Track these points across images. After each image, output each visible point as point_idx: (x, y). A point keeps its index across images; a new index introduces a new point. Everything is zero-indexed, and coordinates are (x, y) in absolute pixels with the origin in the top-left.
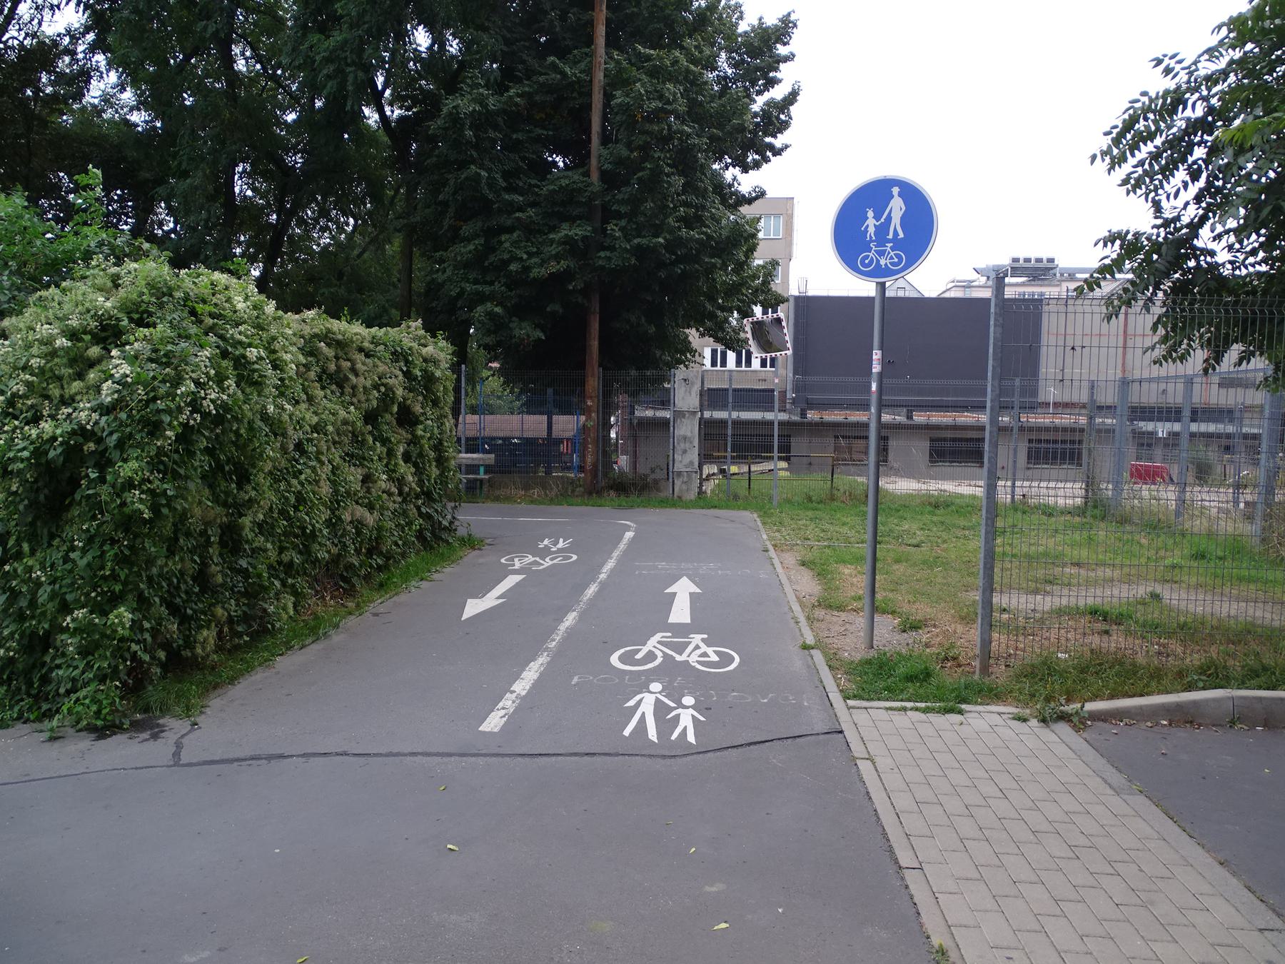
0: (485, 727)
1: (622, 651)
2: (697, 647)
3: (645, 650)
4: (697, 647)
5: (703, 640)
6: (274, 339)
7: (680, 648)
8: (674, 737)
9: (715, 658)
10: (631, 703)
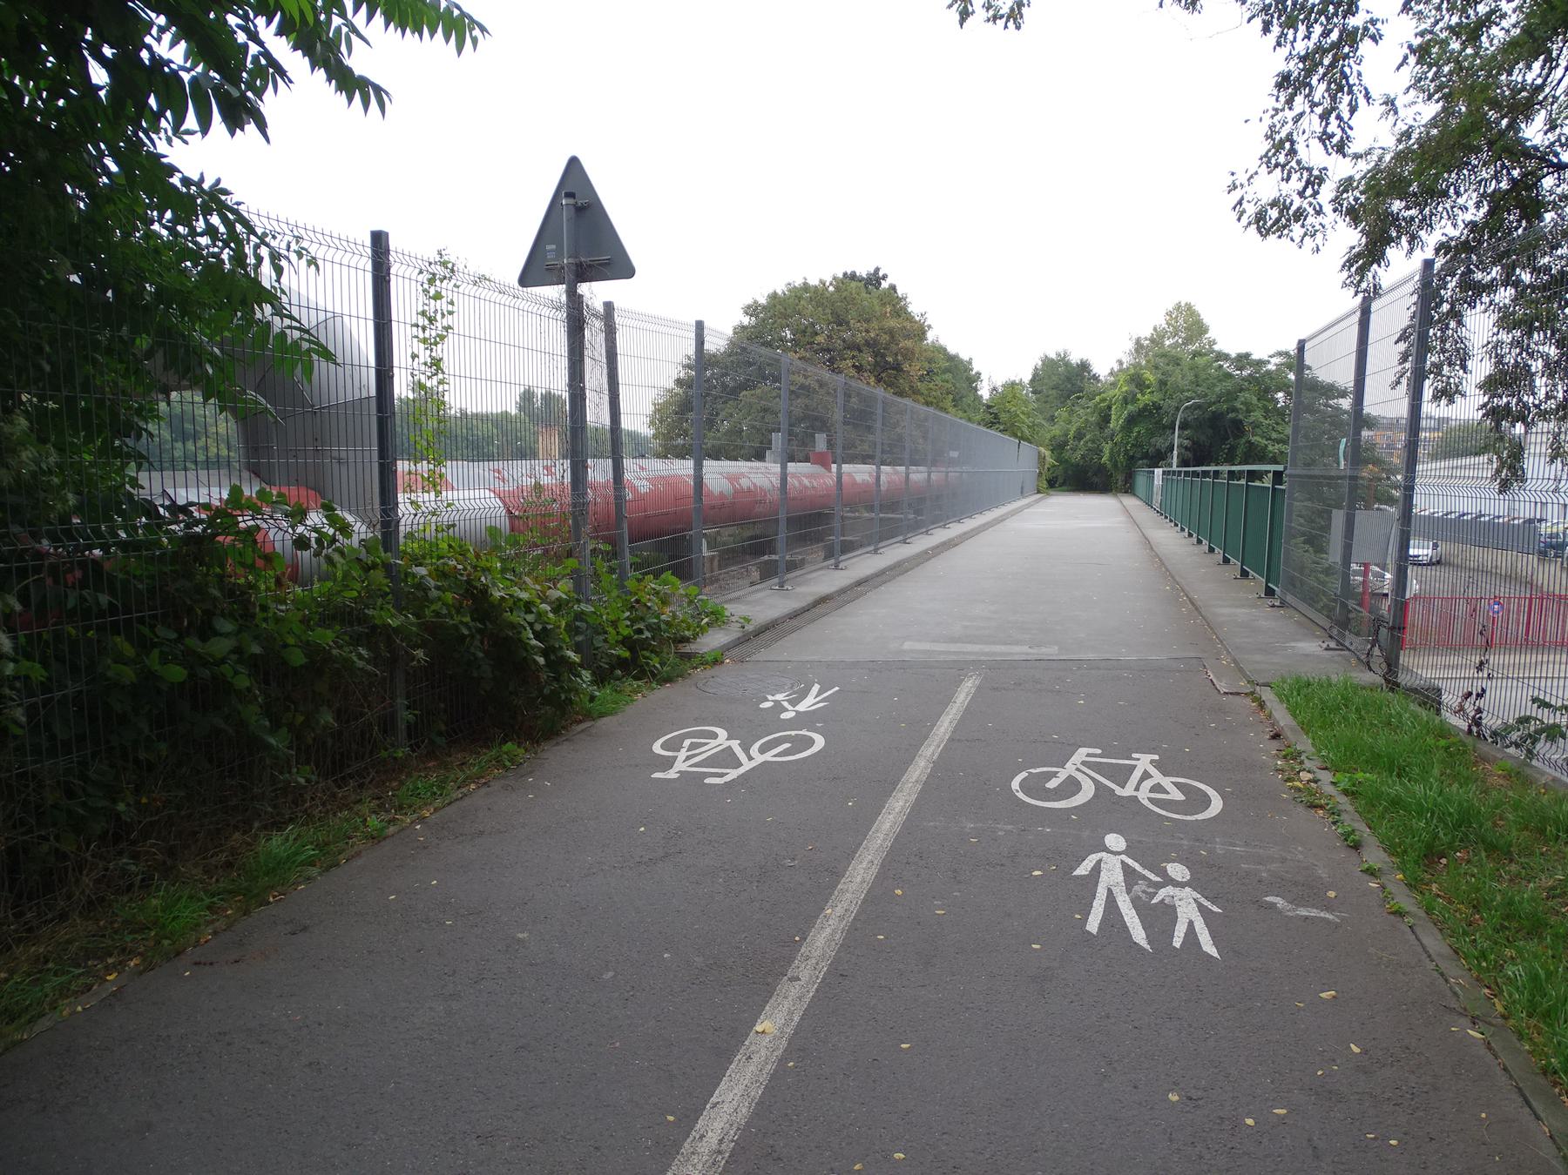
0: (1077, 872)
1: (1200, 817)
2: (1146, 775)
3: (1063, 775)
4: (1146, 775)
5: (1152, 762)
6: (724, 386)
7: (1121, 776)
8: (1177, 943)
9: (1177, 796)
10: (1083, 870)
